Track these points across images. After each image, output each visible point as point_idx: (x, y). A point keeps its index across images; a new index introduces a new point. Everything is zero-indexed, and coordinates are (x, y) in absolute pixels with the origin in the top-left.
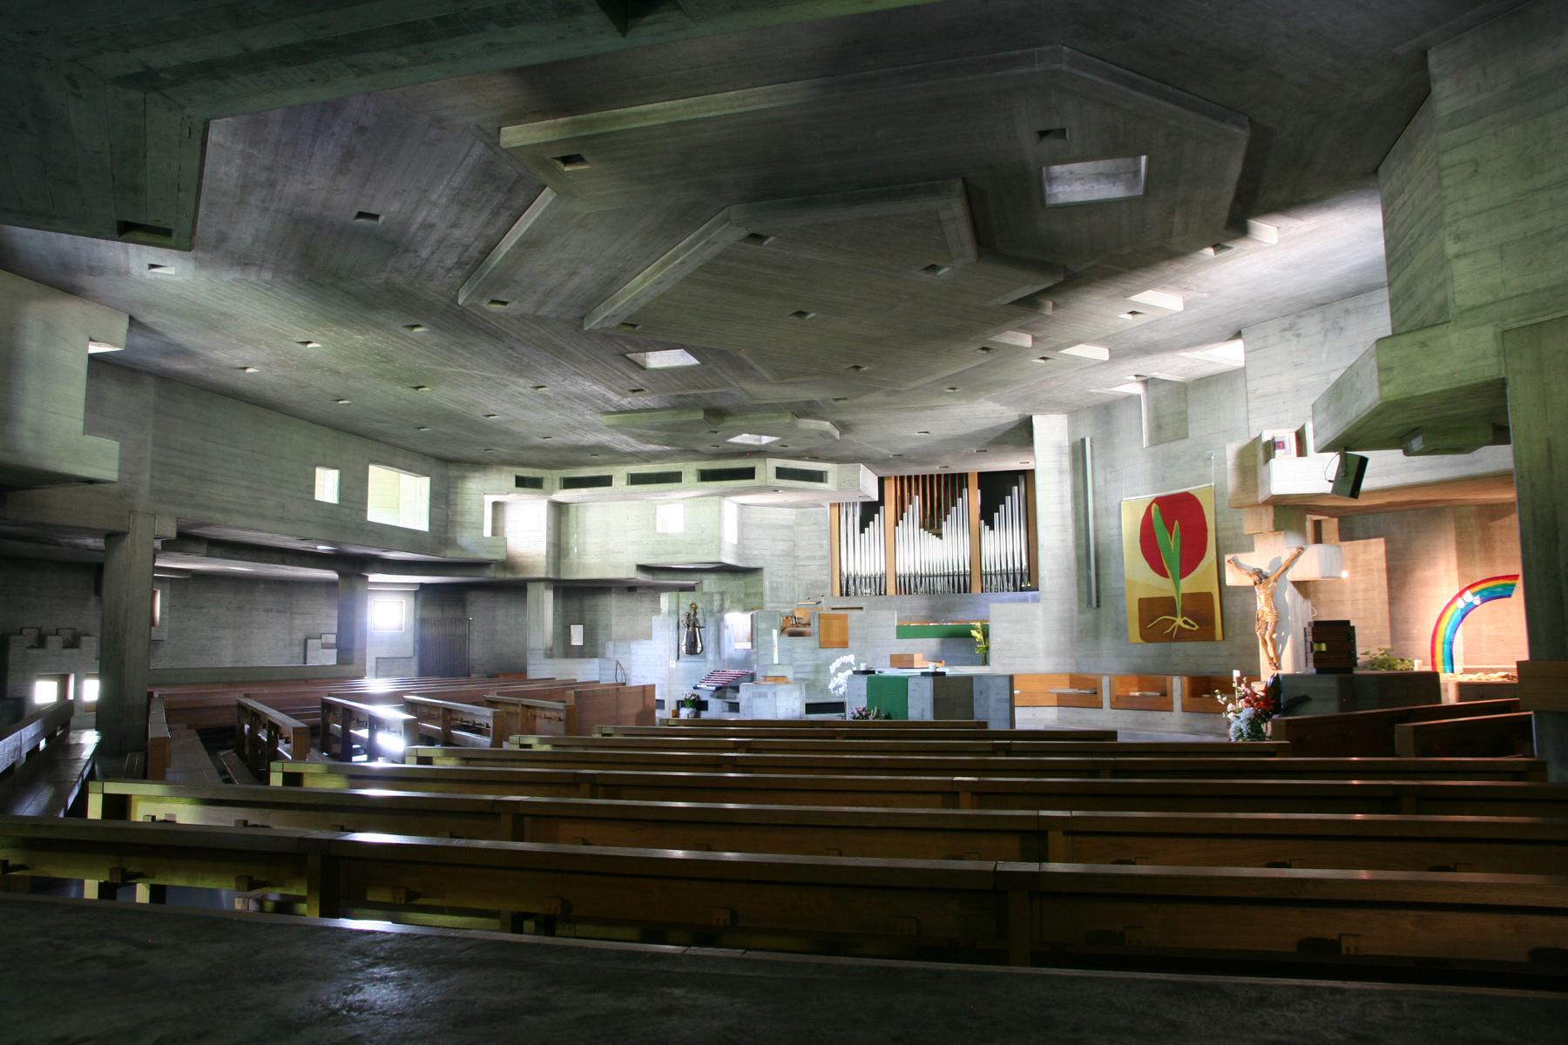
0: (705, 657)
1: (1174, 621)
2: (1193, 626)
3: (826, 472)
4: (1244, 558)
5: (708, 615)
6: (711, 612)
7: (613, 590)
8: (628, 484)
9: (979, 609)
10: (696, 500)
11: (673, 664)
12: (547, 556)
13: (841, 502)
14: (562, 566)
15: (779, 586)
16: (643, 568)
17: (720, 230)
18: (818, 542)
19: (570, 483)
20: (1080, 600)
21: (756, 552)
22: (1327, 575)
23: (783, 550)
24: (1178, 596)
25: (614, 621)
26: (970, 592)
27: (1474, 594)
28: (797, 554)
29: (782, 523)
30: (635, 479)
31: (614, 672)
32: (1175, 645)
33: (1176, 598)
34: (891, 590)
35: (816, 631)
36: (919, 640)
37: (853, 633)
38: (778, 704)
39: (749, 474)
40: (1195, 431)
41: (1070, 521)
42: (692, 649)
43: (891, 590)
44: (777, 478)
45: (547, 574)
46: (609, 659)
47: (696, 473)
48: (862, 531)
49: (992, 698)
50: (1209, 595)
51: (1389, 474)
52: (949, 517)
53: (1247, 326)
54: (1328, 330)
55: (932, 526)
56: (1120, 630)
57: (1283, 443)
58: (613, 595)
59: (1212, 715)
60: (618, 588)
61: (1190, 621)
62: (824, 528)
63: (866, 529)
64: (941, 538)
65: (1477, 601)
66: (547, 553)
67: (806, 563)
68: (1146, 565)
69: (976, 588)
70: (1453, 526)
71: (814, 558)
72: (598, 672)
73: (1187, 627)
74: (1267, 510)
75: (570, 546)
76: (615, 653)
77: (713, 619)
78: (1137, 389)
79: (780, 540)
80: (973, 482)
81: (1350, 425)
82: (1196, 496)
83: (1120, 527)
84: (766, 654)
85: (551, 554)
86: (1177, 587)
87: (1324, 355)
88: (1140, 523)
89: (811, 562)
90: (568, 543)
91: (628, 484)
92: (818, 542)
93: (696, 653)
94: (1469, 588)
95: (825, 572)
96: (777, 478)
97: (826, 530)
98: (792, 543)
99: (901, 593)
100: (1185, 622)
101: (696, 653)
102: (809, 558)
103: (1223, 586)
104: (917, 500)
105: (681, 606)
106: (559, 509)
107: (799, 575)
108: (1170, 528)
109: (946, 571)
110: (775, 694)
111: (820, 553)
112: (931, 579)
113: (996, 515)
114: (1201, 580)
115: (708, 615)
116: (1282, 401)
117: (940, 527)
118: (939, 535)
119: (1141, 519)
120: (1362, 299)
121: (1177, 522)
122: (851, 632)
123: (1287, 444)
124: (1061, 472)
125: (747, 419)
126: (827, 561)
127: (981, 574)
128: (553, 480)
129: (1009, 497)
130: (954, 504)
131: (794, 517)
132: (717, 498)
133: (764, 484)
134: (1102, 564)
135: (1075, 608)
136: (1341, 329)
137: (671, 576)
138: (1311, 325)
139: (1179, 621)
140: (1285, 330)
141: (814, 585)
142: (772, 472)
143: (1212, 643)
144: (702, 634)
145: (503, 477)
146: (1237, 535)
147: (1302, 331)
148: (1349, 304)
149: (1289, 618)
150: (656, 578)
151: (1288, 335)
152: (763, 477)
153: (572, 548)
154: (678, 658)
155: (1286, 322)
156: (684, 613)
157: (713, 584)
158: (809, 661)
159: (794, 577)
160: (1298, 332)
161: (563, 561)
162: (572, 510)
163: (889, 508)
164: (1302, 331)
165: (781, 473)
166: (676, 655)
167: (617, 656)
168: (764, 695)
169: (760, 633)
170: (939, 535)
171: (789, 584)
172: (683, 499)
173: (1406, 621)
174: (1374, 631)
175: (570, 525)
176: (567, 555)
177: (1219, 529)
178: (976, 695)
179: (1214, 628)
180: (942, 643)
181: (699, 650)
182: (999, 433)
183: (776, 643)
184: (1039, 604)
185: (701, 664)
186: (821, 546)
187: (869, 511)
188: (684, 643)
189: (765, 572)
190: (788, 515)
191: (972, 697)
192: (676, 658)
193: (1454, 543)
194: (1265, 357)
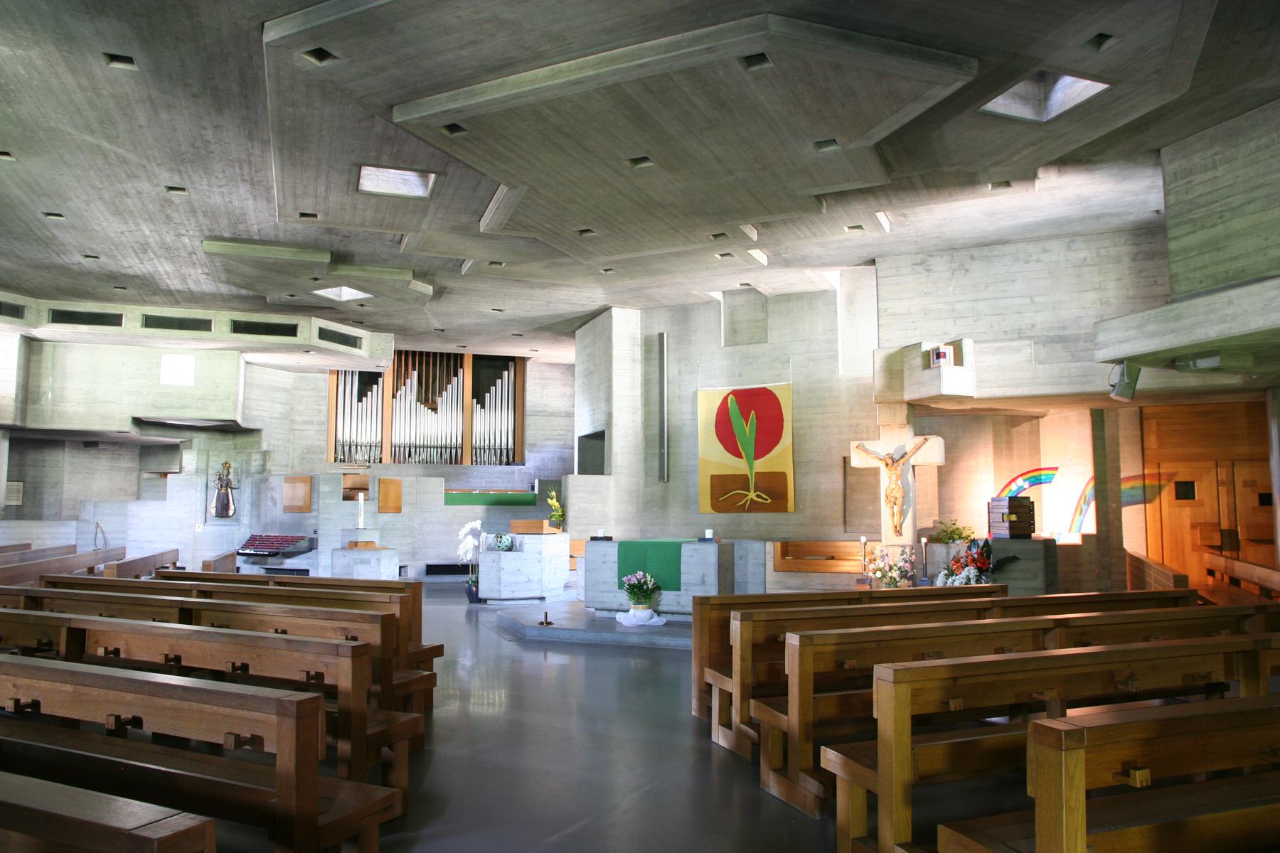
0: (238, 520)
1: (747, 495)
2: (767, 500)
3: (360, 338)
4: (869, 445)
5: (244, 475)
6: (249, 474)
7: (67, 444)
8: (142, 327)
9: (470, 480)
10: (211, 352)
11: (200, 528)
12: (16, 400)
13: (347, 369)
14: (29, 412)
15: (276, 449)
16: (138, 422)
17: (745, 37)
18: (316, 407)
19: (60, 317)
20: (647, 473)
21: (256, 413)
23: (281, 413)
24: (751, 475)
25: (66, 479)
26: (461, 463)
27: (1025, 480)
30: (151, 322)
31: (93, 536)
32: (746, 516)
33: (749, 476)
34: (387, 458)
35: (376, 495)
36: (467, 507)
37: (406, 498)
39: (291, 330)
40: (773, 335)
41: (639, 404)
42: (223, 512)
43: (387, 458)
44: (320, 338)
45: (16, 420)
46: (86, 521)
47: (229, 323)
48: (360, 400)
49: (751, 562)
50: (783, 476)
51: (1018, 386)
52: (444, 393)
53: (882, 256)
54: (955, 270)
56: (689, 503)
57: (944, 353)
58: (66, 450)
59: (804, 574)
60: (72, 442)
61: (762, 495)
62: (324, 394)
63: (364, 399)
64: (436, 412)
65: (1026, 485)
66: (17, 396)
67: (304, 427)
68: (721, 447)
70: (991, 431)
71: (312, 423)
72: (74, 536)
73: (760, 500)
74: (901, 407)
75: (41, 390)
76: (95, 514)
77: (250, 480)
78: (718, 296)
79: (278, 403)
80: (468, 364)
82: (773, 391)
83: (695, 413)
84: (326, 518)
85: (20, 398)
86: (751, 467)
87: (951, 289)
88: (716, 411)
89: (308, 427)
90: (39, 387)
91: (142, 327)
92: (316, 407)
93: (227, 516)
94: (1021, 475)
95: (323, 437)
96: (320, 338)
97: (325, 397)
99: (394, 462)
100: (758, 496)
101: (227, 516)
102: (306, 423)
103: (847, 465)
104: (416, 373)
105: (210, 464)
106: (31, 345)
108: (746, 417)
109: (426, 443)
110: (378, 560)
113: (487, 395)
114: (779, 459)
115: (244, 475)
116: (912, 320)
117: (434, 402)
118: (435, 410)
119: (718, 406)
120: (985, 251)
121: (753, 412)
123: (947, 355)
124: (634, 361)
125: (364, 270)
128: (39, 311)
130: (449, 382)
131: (292, 381)
132: (236, 353)
133: (307, 343)
134: (672, 444)
135: (642, 481)
136: (967, 270)
137: (160, 432)
138: (940, 264)
139: (752, 495)
140: (917, 264)
141: (309, 450)
142: (316, 332)
143: (783, 515)
144: (235, 496)
146: (811, 426)
147: (931, 267)
148: (975, 252)
149: (911, 494)
150: (144, 433)
151: (919, 268)
152: (306, 335)
153: (45, 393)
154: (1070, 532)
155: (918, 258)
156: (214, 472)
157: (202, 443)
158: (370, 525)
160: (928, 267)
161: (31, 407)
162: (48, 349)
163: (388, 381)
164: (931, 267)
165: (324, 334)
166: (203, 519)
167: (97, 519)
168: (368, 562)
169: (321, 496)
170: (435, 410)
171: (285, 447)
172: (195, 350)
173: (952, 500)
174: (925, 506)
175: (44, 365)
176: (37, 400)
177: (1144, 416)
178: (737, 560)
179: (787, 502)
180: (488, 509)
181: (231, 512)
182: (561, 319)
183: (362, 508)
184: (612, 477)
185: (234, 528)
186: (320, 411)
187: (368, 380)
188: (214, 504)
189: (264, 434)
190: (288, 379)
191: (733, 563)
192: (203, 521)
193: (992, 442)
194: (897, 284)
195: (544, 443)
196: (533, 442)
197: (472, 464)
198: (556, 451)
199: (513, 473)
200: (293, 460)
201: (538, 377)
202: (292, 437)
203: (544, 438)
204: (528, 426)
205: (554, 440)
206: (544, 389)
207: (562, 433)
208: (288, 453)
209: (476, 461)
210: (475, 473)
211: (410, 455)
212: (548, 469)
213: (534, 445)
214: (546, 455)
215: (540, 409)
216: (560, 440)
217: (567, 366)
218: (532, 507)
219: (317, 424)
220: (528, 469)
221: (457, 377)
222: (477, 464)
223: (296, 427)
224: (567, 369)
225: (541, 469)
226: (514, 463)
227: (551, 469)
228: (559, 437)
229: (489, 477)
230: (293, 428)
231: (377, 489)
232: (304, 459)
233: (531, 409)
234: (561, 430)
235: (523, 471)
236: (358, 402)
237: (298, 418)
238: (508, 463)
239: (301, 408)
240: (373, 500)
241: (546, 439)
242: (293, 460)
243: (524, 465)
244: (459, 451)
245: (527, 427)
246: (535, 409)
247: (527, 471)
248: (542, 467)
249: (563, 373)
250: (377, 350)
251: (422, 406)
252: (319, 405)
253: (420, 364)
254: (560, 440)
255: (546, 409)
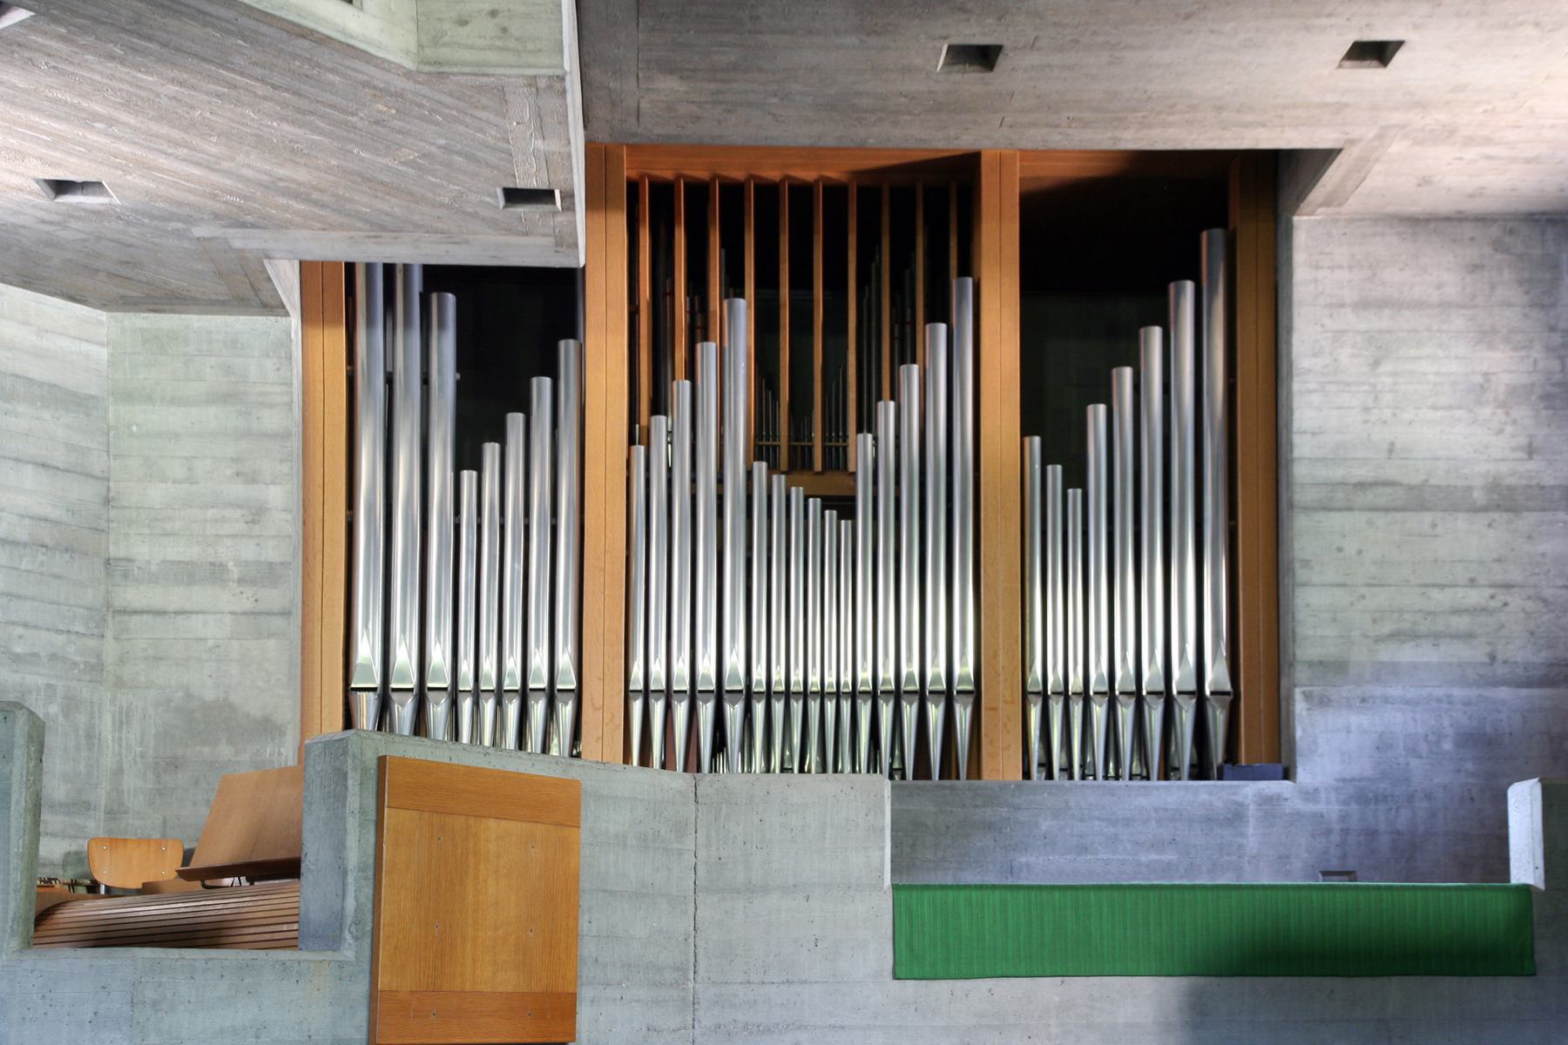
18: (238, 490)
22: (1334, 865)
26: (975, 771)
28: (114, 551)
29: (37, 371)
35: (356, 898)
36: (1048, 990)
38: (458, 989)
48: (467, 457)
55: (799, 463)
62: (273, 420)
63: (491, 450)
67: (175, 597)
69: (1002, 764)
71: (216, 573)
81: (1290, 634)
89: (201, 596)
92: (238, 490)
97: (285, 435)
98: (88, 492)
99: (645, 760)
102: (186, 574)
104: (744, 310)
107: (122, 660)
111: (248, 551)
112: (814, 706)
117: (837, 459)
122: (592, 921)
126: (286, 594)
127: (1025, 694)
129: (1102, 408)
130: (906, 351)
131: (103, 354)
145: (304, 842)
159: (96, 669)
180: (1198, 1014)
186: (256, 514)
195: (1386, 653)
196: (1330, 651)
197: (1027, 775)
198: (1450, 700)
199: (1236, 817)
200: (119, 771)
201: (1348, 295)
202: (110, 649)
203: (1386, 629)
204: (1306, 563)
205: (1436, 637)
206: (1376, 363)
207: (1474, 597)
208: (91, 736)
209: (1047, 765)
210: (1046, 824)
211: (719, 744)
212: (1411, 798)
213: (1335, 668)
214: (1397, 721)
215: (1361, 473)
216: (1469, 636)
217: (1494, 231)
218: (1508, 986)
219: (241, 581)
220: (1310, 795)
221: (946, 319)
222: (1050, 776)
223: (132, 595)
224: (1497, 245)
225: (1379, 798)
226: (1233, 765)
227: (1429, 796)
228: (1462, 623)
229: (1114, 840)
230: (118, 603)
231: (357, 848)
232: (174, 764)
233: (1323, 473)
234: (1472, 583)
235: (1287, 807)
236: (458, 468)
237: (143, 551)
238: (1201, 771)
239: (156, 494)
240: (331, 940)
241: (1398, 636)
242: (119, 771)
243: (1287, 774)
244: (963, 715)
245: (1301, 574)
246: (1337, 473)
247: (1309, 808)
248: (1383, 786)
249: (1475, 268)
250: (463, 23)
251: (779, 481)
252: (252, 479)
253: (767, 280)
254: (1469, 636)
255: (1392, 472)
